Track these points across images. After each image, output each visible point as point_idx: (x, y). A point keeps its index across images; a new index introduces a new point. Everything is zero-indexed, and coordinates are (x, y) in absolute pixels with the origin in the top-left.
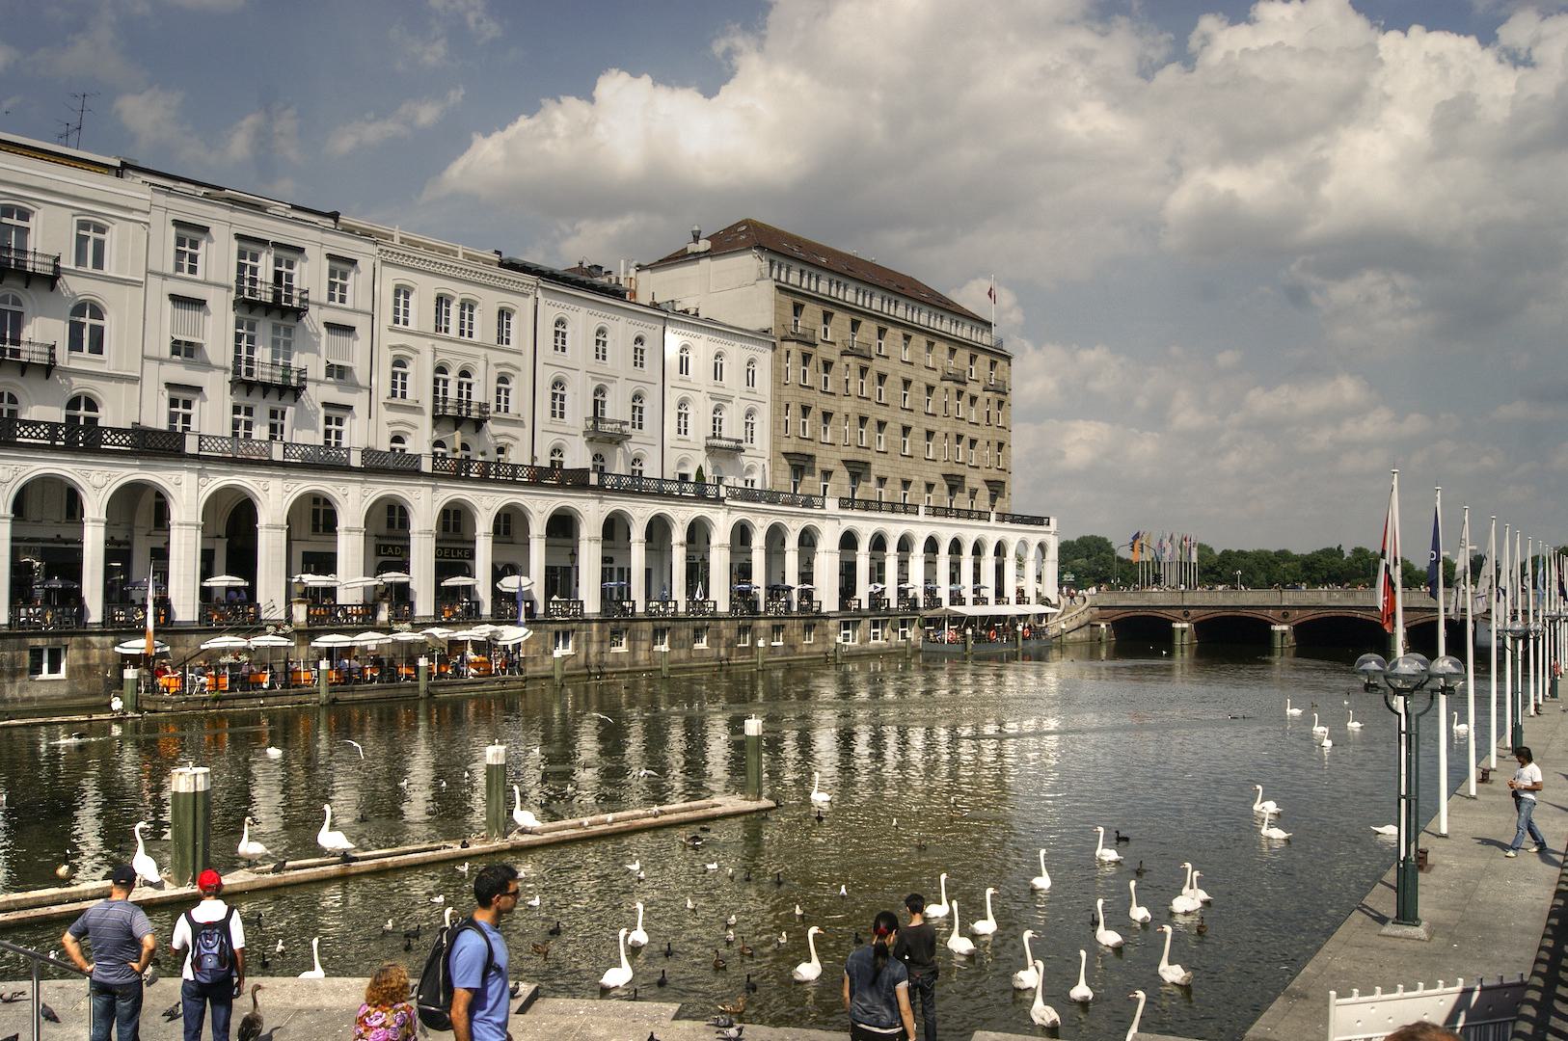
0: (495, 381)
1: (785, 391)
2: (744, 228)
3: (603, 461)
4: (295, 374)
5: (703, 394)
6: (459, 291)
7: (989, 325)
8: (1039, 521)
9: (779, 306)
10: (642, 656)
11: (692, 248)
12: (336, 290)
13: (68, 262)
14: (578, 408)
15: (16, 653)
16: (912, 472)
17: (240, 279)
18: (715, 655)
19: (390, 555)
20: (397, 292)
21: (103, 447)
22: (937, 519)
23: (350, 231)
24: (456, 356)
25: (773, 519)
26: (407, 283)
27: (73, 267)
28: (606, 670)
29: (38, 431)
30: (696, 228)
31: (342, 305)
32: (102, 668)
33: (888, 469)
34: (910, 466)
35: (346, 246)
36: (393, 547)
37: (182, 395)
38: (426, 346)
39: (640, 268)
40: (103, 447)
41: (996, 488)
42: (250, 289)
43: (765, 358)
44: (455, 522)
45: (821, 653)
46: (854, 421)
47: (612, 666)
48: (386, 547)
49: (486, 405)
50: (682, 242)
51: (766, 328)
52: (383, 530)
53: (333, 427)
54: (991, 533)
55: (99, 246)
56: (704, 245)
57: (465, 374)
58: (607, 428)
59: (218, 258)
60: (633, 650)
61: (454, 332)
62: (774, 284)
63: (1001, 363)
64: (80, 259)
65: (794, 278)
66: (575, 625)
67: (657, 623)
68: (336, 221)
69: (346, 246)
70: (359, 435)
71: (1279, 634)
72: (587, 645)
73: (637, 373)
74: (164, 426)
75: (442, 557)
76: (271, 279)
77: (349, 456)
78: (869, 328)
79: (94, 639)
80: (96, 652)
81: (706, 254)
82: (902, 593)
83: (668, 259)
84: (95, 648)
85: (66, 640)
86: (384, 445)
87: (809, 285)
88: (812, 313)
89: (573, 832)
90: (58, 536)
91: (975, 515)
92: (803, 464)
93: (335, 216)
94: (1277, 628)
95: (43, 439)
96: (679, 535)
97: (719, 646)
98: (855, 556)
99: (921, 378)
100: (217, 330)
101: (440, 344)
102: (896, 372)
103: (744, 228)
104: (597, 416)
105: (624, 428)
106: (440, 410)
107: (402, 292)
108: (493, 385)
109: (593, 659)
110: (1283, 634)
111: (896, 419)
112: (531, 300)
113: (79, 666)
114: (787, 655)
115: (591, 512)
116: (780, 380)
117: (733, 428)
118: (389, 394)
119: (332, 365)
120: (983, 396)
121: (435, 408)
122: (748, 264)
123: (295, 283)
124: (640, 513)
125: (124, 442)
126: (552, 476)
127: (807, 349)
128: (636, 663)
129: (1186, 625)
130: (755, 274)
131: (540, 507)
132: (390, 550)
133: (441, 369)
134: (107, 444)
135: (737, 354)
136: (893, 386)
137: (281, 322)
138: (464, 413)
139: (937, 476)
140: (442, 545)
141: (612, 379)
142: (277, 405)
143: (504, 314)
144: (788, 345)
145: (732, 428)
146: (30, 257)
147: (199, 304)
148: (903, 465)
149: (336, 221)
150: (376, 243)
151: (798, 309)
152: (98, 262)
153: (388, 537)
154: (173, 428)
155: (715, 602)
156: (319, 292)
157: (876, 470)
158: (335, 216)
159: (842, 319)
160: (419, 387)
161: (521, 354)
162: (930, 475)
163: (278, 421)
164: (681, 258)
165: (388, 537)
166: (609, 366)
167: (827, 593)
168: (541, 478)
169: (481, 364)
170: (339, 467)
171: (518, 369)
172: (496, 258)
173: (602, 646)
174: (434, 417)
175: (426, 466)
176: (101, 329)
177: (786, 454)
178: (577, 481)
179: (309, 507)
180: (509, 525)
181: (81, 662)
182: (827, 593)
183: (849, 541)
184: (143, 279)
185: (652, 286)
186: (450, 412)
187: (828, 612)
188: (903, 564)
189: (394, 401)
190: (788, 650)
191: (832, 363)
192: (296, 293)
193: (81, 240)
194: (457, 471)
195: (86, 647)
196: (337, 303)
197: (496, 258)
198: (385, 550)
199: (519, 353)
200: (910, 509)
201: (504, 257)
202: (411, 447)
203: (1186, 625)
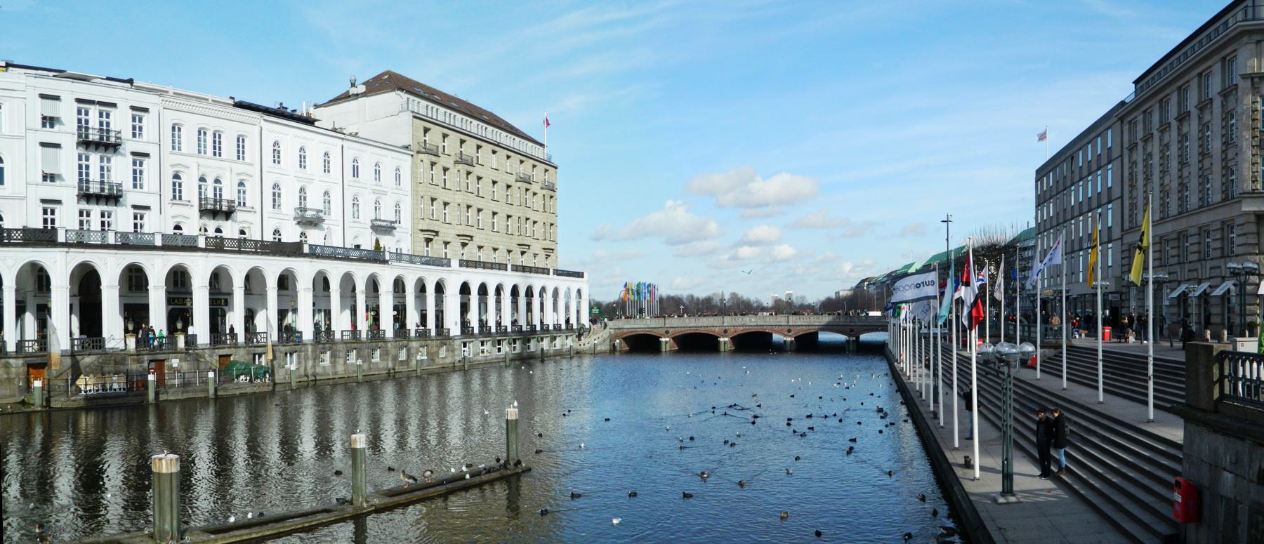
0: (237, 185)
1: (420, 188)
2: (386, 77)
3: (280, 235)
4: (115, 188)
6: (211, 125)
9: (415, 129)
11: (353, 91)
12: (136, 131)
14: (290, 203)
16: (499, 243)
18: (386, 366)
19: (176, 304)
23: (139, 88)
24: (212, 168)
28: (318, 378)
29: (17, 235)
30: (353, 78)
33: (484, 241)
34: (497, 239)
35: (141, 99)
36: (178, 299)
37: (50, 204)
39: (316, 106)
41: (549, 252)
42: (85, 134)
43: (405, 162)
44: (218, 279)
45: (450, 363)
47: (321, 375)
48: (174, 299)
49: (233, 202)
50: (344, 87)
51: (406, 144)
52: (172, 289)
53: (138, 221)
54: (551, 282)
56: (362, 89)
57: (217, 181)
58: (309, 214)
59: (67, 111)
60: (334, 363)
62: (411, 115)
65: (423, 111)
68: (132, 85)
69: (141, 99)
70: (157, 225)
71: (723, 343)
72: (305, 361)
73: (325, 177)
74: (40, 226)
75: (213, 305)
76: (97, 126)
77: (154, 239)
78: (471, 144)
79: (12, 361)
81: (364, 94)
82: (499, 324)
83: (330, 101)
84: (13, 367)
86: (171, 231)
87: (432, 115)
88: (435, 136)
89: (359, 480)
91: (539, 270)
92: (432, 237)
93: (130, 81)
94: (722, 339)
96: (361, 287)
97: (387, 360)
98: (487, 298)
99: (503, 179)
100: (67, 160)
101: (202, 161)
102: (488, 175)
103: (386, 77)
105: (321, 214)
106: (203, 206)
107: (176, 128)
108: (236, 188)
109: (310, 371)
110: (725, 343)
111: (489, 207)
112: (257, 129)
114: (430, 365)
115: (305, 271)
116: (416, 183)
118: (172, 197)
120: (516, 185)
121: (200, 205)
122: (394, 99)
123: (112, 127)
124: (238, 267)
125: (19, 237)
126: (278, 248)
128: (336, 373)
129: (668, 339)
130: (398, 108)
131: (272, 267)
132: (176, 301)
133: (202, 179)
134: (15, 240)
135: (390, 161)
136: (486, 182)
137: (105, 155)
138: (218, 207)
140: (172, 296)
142: (105, 208)
144: (421, 156)
145: (387, 215)
148: (494, 238)
149: (132, 85)
150: (160, 96)
153: (175, 293)
154: (46, 227)
155: (384, 331)
156: (127, 134)
157: (478, 240)
158: (130, 81)
159: (454, 138)
160: (190, 191)
161: (171, 166)
163: (106, 219)
164: (346, 97)
165: (175, 293)
166: (332, 176)
167: (452, 323)
168: (278, 248)
169: (228, 174)
172: (231, 102)
174: (200, 211)
175: (201, 243)
177: (422, 231)
178: (294, 250)
179: (28, 268)
180: (253, 281)
182: (452, 323)
183: (465, 289)
185: (326, 117)
186: (209, 207)
187: (454, 336)
188: (498, 302)
189: (174, 201)
190: (431, 362)
191: (448, 169)
192: (113, 134)
194: (218, 246)
196: (137, 139)
197: (231, 102)
198: (173, 301)
199: (251, 164)
200: (502, 267)
201: (236, 100)
202: (186, 231)
203: (668, 339)
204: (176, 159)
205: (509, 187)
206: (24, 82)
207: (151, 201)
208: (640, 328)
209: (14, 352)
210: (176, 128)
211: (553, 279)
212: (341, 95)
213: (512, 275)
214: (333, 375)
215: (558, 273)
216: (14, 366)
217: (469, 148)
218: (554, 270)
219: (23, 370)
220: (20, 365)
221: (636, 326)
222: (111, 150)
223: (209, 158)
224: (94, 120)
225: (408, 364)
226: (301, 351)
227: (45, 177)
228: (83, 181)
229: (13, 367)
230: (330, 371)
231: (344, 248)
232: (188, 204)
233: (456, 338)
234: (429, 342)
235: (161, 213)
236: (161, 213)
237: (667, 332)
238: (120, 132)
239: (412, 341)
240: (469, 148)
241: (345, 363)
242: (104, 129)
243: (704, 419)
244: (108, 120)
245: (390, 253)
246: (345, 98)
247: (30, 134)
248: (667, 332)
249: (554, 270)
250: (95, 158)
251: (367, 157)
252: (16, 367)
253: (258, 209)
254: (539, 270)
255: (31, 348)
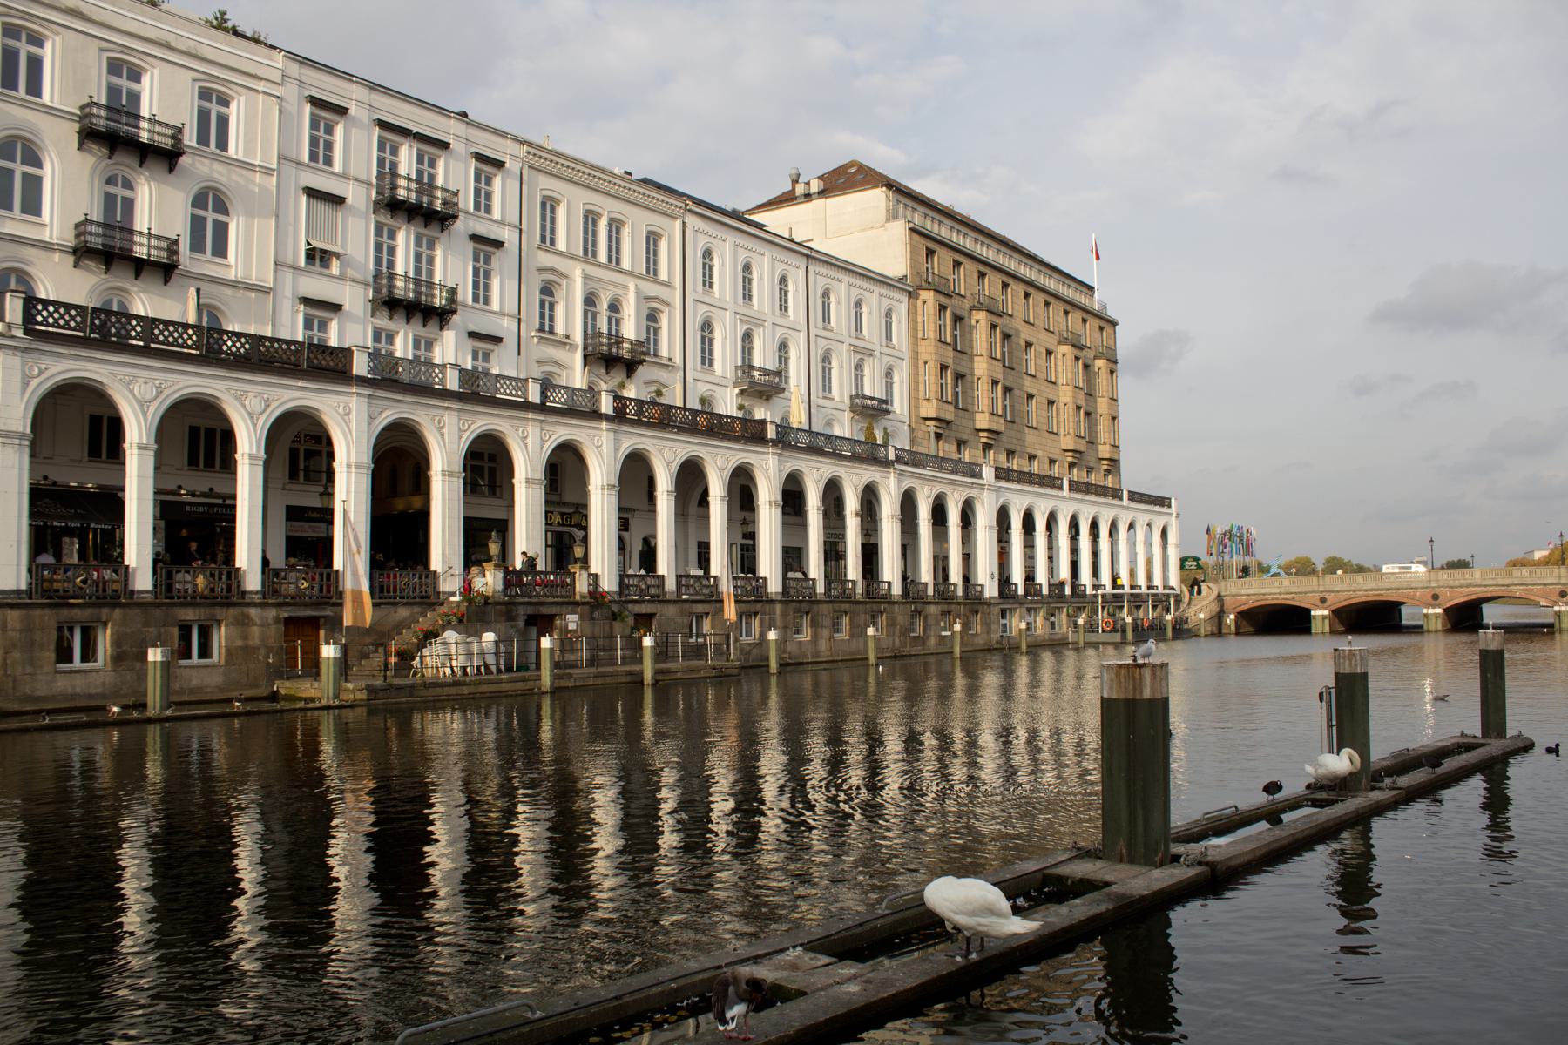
2: (853, 170)
5: (845, 347)
7: (1091, 289)
8: (1162, 502)
9: (913, 252)
10: (823, 646)
13: (190, 139)
15: (162, 630)
17: (380, 176)
20: (543, 205)
21: (152, 345)
22: (1079, 496)
25: (866, 479)
26: (554, 195)
27: (196, 145)
31: (487, 216)
32: (262, 651)
38: (577, 272)
40: (152, 345)
43: (902, 307)
46: (1071, 406)
55: (223, 122)
60: (815, 638)
61: (602, 256)
63: (1108, 328)
64: (203, 139)
66: (759, 606)
67: (836, 606)
71: (1321, 619)
79: (253, 611)
80: (255, 630)
84: (254, 624)
85: (219, 612)
90: (211, 489)
95: (74, 329)
103: (853, 170)
104: (747, 367)
106: (590, 349)
112: (678, 224)
113: (236, 648)
117: (763, 358)
119: (314, 249)
122: (875, 199)
127: (944, 300)
128: (817, 654)
135: (875, 301)
139: (1058, 451)
141: (760, 322)
143: (653, 238)
145: (872, 387)
146: (144, 124)
147: (338, 201)
151: (930, 253)
152: (223, 144)
160: (570, 319)
162: (1052, 450)
169: (632, 296)
170: (424, 390)
171: (668, 304)
173: (786, 632)
176: (38, 180)
179: (1528, 743)
181: (239, 643)
183: (1003, 517)
184: (275, 167)
185: (775, 220)
187: (990, 598)
193: (203, 116)
195: (243, 622)
199: (668, 285)
200: (1052, 482)
204: (546, 259)
205: (1049, 353)
206: (280, 67)
207: (506, 327)
208: (1270, 594)
209: (257, 593)
210: (549, 205)
211: (1071, 498)
212: (779, 197)
213: (1071, 498)
214: (812, 657)
215: (1135, 497)
216: (258, 622)
217: (993, 282)
218: (1129, 492)
219: (275, 632)
220: (270, 621)
221: (1263, 591)
222: (436, 226)
223: (600, 265)
224: (406, 159)
225: (924, 644)
226: (764, 613)
227: (311, 254)
228: (383, 274)
229: (254, 624)
230: (809, 651)
231: (810, 432)
232: (566, 341)
233: (992, 601)
234: (953, 607)
235: (519, 354)
236: (519, 354)
237: (1323, 600)
238: (456, 194)
239: (930, 603)
240: (993, 282)
241: (831, 638)
242: (425, 184)
243: (1073, 682)
244: (427, 354)
245: (896, 449)
246: (787, 200)
247: (290, 170)
248: (1323, 600)
249: (1129, 492)
250: (404, 239)
251: (843, 291)
252: (262, 625)
253: (678, 360)
254: (1100, 490)
255: (292, 586)
